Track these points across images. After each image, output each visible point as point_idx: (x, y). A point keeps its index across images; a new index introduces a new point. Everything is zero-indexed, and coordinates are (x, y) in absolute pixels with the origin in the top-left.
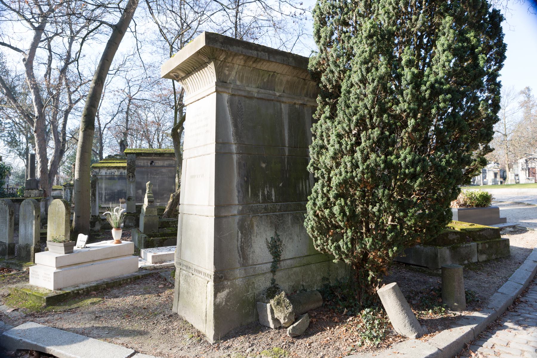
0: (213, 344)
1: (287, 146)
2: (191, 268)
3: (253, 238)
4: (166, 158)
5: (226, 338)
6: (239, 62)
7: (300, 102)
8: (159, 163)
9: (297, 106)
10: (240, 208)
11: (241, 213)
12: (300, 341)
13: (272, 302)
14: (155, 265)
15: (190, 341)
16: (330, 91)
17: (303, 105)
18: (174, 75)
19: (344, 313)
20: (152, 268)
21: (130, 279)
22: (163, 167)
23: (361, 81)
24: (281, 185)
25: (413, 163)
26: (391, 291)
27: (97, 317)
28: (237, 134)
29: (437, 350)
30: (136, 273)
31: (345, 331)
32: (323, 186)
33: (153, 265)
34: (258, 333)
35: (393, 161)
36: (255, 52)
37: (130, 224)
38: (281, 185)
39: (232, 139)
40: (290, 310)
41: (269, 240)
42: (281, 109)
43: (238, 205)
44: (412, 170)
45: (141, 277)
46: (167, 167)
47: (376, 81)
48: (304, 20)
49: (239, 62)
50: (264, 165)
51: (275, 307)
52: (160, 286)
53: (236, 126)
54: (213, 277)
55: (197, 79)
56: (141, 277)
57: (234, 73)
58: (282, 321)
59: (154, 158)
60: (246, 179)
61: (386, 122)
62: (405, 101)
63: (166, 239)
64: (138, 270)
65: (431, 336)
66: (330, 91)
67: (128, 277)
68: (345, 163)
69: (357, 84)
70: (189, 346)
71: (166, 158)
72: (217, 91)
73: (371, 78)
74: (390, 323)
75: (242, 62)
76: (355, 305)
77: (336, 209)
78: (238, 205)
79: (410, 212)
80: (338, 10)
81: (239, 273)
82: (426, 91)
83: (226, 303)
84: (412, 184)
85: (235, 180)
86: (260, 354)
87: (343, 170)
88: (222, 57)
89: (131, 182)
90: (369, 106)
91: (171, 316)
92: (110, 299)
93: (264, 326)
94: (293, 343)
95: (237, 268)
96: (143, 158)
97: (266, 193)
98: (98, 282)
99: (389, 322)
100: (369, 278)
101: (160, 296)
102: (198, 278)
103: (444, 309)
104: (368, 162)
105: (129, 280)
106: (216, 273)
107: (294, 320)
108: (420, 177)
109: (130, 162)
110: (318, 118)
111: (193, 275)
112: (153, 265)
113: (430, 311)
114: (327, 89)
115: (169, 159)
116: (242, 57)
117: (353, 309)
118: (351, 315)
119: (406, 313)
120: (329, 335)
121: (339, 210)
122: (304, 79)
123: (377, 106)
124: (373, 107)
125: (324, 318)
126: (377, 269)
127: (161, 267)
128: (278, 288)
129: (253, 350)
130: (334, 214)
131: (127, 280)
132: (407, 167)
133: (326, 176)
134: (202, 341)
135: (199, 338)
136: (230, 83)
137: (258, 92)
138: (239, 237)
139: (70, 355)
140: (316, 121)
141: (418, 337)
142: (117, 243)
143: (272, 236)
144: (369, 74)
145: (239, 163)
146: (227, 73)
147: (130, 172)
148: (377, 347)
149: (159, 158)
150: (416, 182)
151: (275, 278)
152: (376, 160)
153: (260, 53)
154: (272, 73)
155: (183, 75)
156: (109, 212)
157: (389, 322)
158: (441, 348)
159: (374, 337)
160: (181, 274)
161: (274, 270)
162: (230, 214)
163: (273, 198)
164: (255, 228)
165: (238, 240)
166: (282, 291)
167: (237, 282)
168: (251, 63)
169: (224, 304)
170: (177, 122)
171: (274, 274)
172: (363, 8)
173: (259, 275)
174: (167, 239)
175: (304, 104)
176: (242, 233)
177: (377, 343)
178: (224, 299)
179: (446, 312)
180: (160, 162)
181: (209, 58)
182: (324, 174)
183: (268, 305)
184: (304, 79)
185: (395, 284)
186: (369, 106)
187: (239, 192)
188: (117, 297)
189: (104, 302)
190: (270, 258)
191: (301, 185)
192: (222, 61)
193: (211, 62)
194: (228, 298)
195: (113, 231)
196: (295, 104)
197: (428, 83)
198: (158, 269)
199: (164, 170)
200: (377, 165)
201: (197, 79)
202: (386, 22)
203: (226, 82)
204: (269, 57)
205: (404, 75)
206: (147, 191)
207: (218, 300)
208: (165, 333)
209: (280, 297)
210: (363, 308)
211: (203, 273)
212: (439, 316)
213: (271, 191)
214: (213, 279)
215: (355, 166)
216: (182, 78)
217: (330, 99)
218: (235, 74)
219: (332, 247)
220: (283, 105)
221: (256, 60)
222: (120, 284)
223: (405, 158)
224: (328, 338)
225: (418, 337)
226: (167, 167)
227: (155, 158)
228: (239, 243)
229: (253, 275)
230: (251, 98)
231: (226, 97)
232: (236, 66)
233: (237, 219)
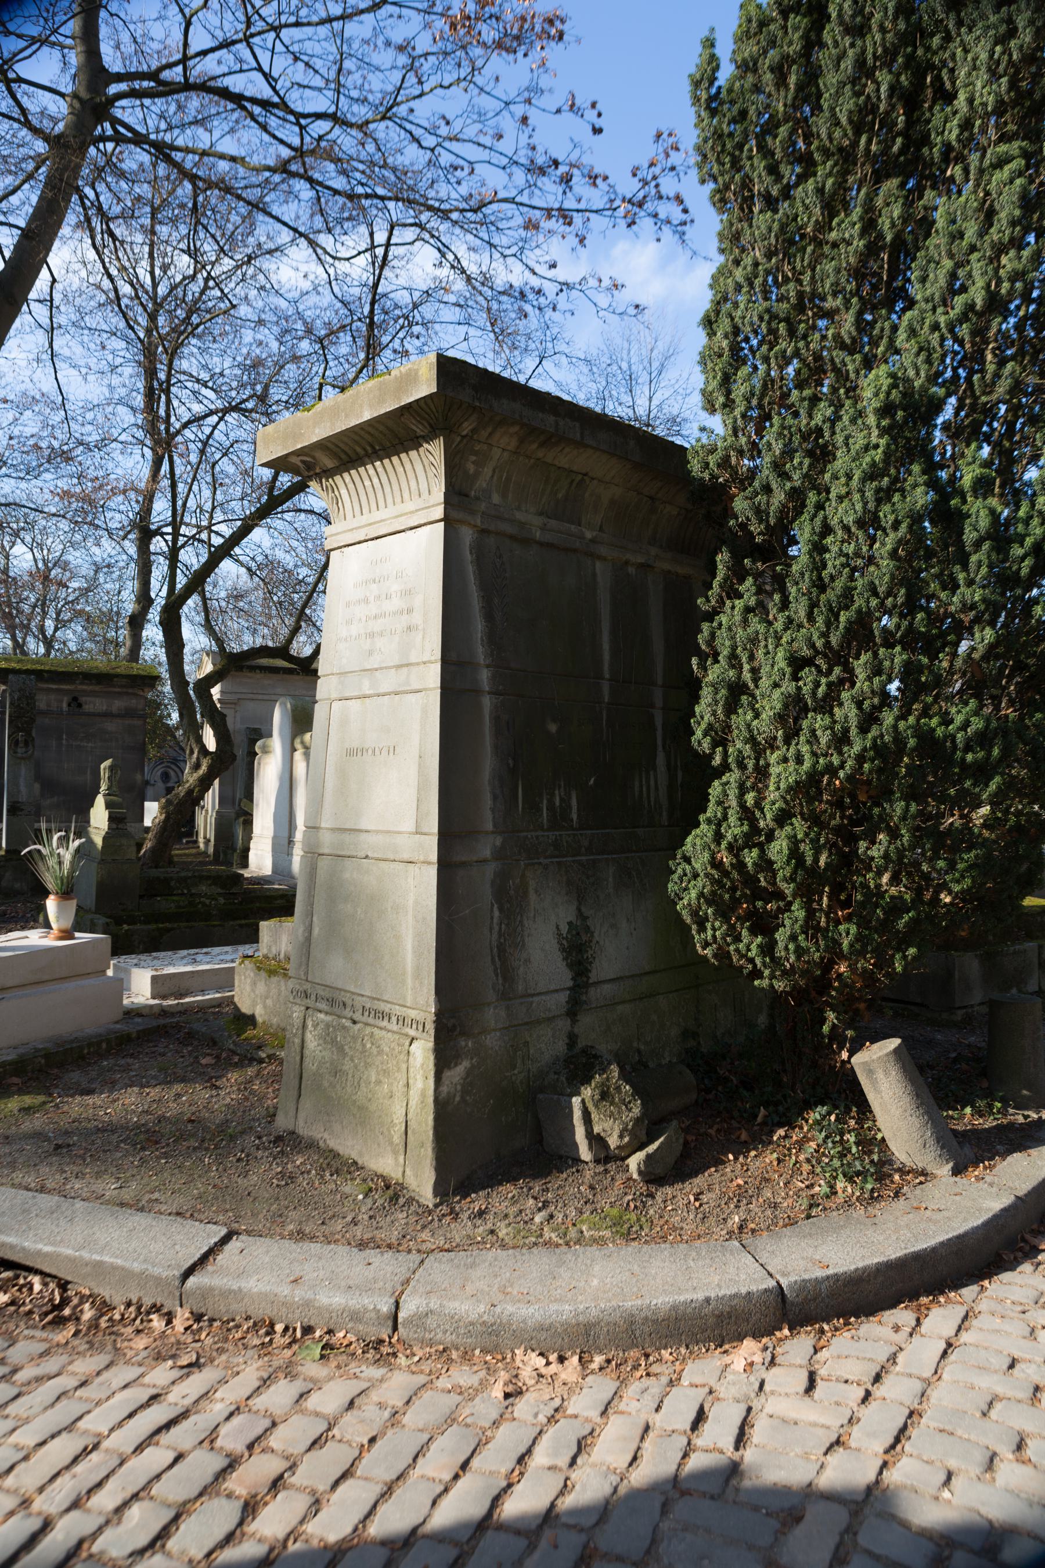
0: (436, 1206)
1: (607, 676)
2: (349, 1003)
3: (526, 923)
4: (117, 690)
5: (465, 1189)
6: (504, 441)
7: (640, 559)
8: (94, 704)
9: (631, 570)
10: (498, 841)
11: (499, 855)
12: (669, 1190)
13: (587, 1092)
14: (165, 1003)
15: (369, 1201)
16: (759, 539)
17: (645, 567)
18: (303, 462)
19: (759, 1119)
20: (156, 1010)
21: (108, 1041)
22: (107, 715)
23: (861, 523)
24: (592, 782)
25: (983, 739)
26: (892, 1058)
27: (58, 1147)
28: (493, 639)
29: (1013, 1198)
30: (118, 1026)
31: (775, 1163)
32: (742, 790)
33: (156, 1002)
34: (549, 1174)
35: (934, 730)
36: (552, 419)
37: (17, 886)
38: (592, 782)
39: (480, 653)
40: (636, 1110)
41: (564, 930)
42: (594, 575)
43: (493, 832)
44: (981, 754)
45: (134, 1035)
46: (119, 716)
47: (904, 525)
48: (549, 313)
49: (504, 441)
50: (553, 728)
51: (596, 1106)
52: (204, 1061)
53: (489, 616)
54: (431, 1027)
55: (375, 480)
56: (134, 1035)
57: (487, 471)
58: (613, 1142)
59: (80, 687)
60: (511, 762)
61: (920, 632)
62: (970, 583)
63: (169, 930)
64: (120, 1016)
65: (985, 1168)
66: (759, 539)
67: (100, 1035)
68: (813, 732)
69: (846, 528)
70: (371, 1213)
71: (117, 690)
72: (447, 519)
73: (891, 518)
74: (883, 1139)
75: (514, 443)
76: (784, 1097)
77: (778, 849)
78: (493, 832)
79: (962, 859)
80: (782, 328)
81: (493, 1016)
82: (1023, 559)
83: (462, 1097)
84: (977, 790)
85: (488, 765)
86: (574, 1225)
87: (805, 749)
88: (466, 428)
89: (23, 758)
90: (882, 590)
91: (279, 1139)
92: (72, 1096)
93: (561, 1157)
94: (652, 1196)
95: (489, 1004)
96: (45, 686)
97: (557, 803)
98: (21, 1051)
99: (879, 1136)
100: (826, 1029)
101: (217, 1088)
102: (376, 1031)
103: (999, 1105)
104: (874, 732)
105: (104, 1045)
106: (439, 1014)
107: (644, 1138)
108: (998, 773)
109: (19, 699)
110: (714, 608)
111: (354, 1022)
112: (156, 1002)
113: (968, 1110)
114: (751, 534)
115: (127, 694)
116: (515, 429)
117: (781, 1108)
118: (781, 1125)
119: (927, 1112)
120: (737, 1173)
121: (786, 852)
122: (651, 498)
123: (903, 591)
124: (889, 593)
125: (712, 1132)
126: (847, 1007)
127: (179, 1008)
128: (596, 1057)
129: (551, 1216)
130: (771, 863)
131: (99, 1044)
132: (968, 748)
133: (750, 764)
134: (402, 1201)
135: (390, 1192)
136: (477, 498)
137: (543, 528)
138: (495, 921)
139: (40, 1246)
140: (710, 616)
141: (957, 1171)
142: (61, 938)
143: (569, 919)
144: (886, 508)
145: (496, 720)
146: (471, 468)
147: (20, 730)
148: (872, 1198)
149: (97, 688)
150: (987, 786)
151: (576, 1030)
152: (895, 727)
153: (561, 423)
154: (580, 477)
155: (329, 463)
156: (38, 847)
157: (879, 1136)
158: (1021, 1193)
159: (858, 1174)
160: (309, 1023)
161: (574, 1008)
162: (475, 859)
163: (575, 816)
164: (532, 896)
165: (491, 929)
166: (610, 1064)
167: (488, 1042)
168: (534, 446)
169: (457, 1099)
170: (179, 586)
171: (574, 1022)
172: (853, 329)
173: (539, 1022)
174: (172, 929)
175: (649, 566)
176: (501, 910)
177: (869, 1186)
178: (459, 1087)
179: (1003, 1112)
180: (98, 701)
181: (431, 426)
182: (744, 758)
183: (576, 1101)
184: (651, 498)
185: (895, 1043)
186: (882, 590)
187: (495, 798)
188: (89, 1092)
189: (57, 1106)
190: (564, 977)
191: (637, 784)
192: (464, 437)
193: (436, 437)
194: (468, 1085)
195: (51, 904)
196: (627, 563)
197: (1029, 541)
198: (173, 1015)
199: (111, 726)
200: (899, 740)
201: (375, 480)
202: (923, 374)
203: (467, 496)
204: (582, 434)
205: (969, 516)
206: (103, 787)
207: (444, 1089)
208: (287, 1184)
209: (608, 1079)
210: (810, 1106)
211: (394, 1019)
212: (989, 1123)
213: (570, 798)
214: (432, 1032)
215: (841, 740)
216: (324, 471)
217: (754, 562)
218: (490, 474)
219: (754, 947)
220: (598, 565)
221: (551, 440)
222: (82, 1057)
223: (966, 724)
224: (740, 1181)
225: (957, 1171)
226: (119, 716)
227: (85, 687)
228: (495, 936)
229: (526, 1024)
230: (526, 542)
231: (467, 535)
232: (496, 453)
233: (490, 870)
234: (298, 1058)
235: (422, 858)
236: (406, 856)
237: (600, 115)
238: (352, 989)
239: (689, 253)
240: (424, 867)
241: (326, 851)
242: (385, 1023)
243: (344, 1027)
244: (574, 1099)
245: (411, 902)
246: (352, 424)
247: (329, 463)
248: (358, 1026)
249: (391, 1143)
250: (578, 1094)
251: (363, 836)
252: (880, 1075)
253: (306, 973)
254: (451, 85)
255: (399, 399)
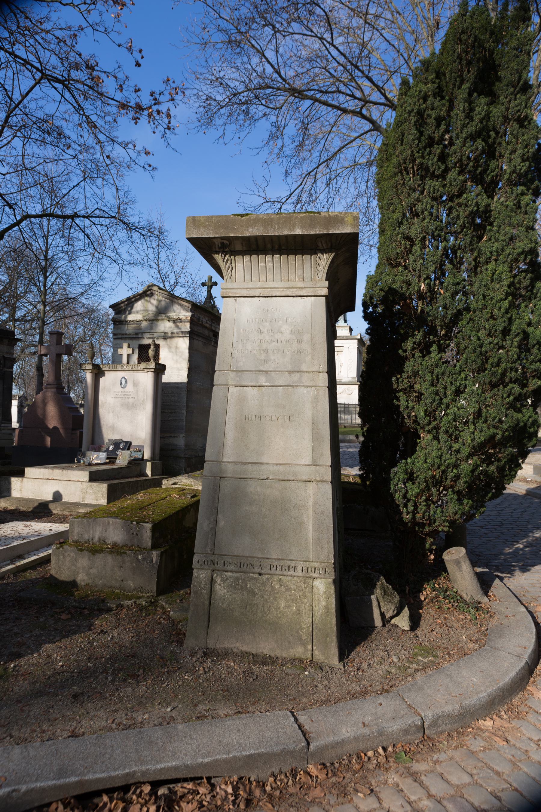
155: (238, 247)
183: (372, 597)
234: (207, 602)
235: (318, 479)
236: (304, 478)
237: (142, 57)
238: (259, 555)
239: (166, 144)
240: (320, 485)
241: (229, 475)
242: (292, 572)
243: (253, 578)
244: (372, 597)
245: (311, 502)
246: (271, 234)
247: (238, 247)
248: (265, 577)
249: (300, 639)
250: (373, 594)
251: (264, 467)
252: (463, 564)
253: (213, 550)
254: (67, 4)
255: (327, 229)
